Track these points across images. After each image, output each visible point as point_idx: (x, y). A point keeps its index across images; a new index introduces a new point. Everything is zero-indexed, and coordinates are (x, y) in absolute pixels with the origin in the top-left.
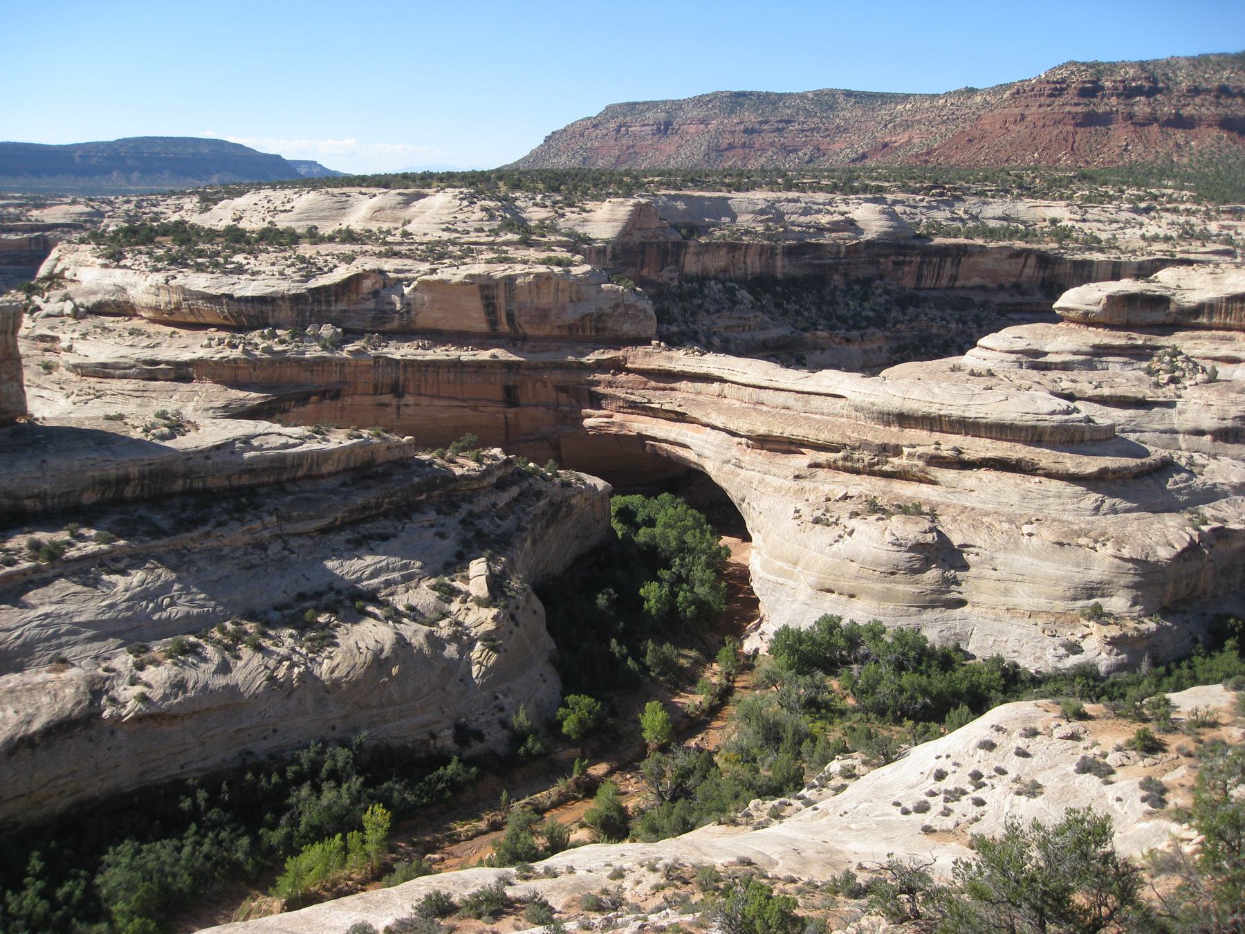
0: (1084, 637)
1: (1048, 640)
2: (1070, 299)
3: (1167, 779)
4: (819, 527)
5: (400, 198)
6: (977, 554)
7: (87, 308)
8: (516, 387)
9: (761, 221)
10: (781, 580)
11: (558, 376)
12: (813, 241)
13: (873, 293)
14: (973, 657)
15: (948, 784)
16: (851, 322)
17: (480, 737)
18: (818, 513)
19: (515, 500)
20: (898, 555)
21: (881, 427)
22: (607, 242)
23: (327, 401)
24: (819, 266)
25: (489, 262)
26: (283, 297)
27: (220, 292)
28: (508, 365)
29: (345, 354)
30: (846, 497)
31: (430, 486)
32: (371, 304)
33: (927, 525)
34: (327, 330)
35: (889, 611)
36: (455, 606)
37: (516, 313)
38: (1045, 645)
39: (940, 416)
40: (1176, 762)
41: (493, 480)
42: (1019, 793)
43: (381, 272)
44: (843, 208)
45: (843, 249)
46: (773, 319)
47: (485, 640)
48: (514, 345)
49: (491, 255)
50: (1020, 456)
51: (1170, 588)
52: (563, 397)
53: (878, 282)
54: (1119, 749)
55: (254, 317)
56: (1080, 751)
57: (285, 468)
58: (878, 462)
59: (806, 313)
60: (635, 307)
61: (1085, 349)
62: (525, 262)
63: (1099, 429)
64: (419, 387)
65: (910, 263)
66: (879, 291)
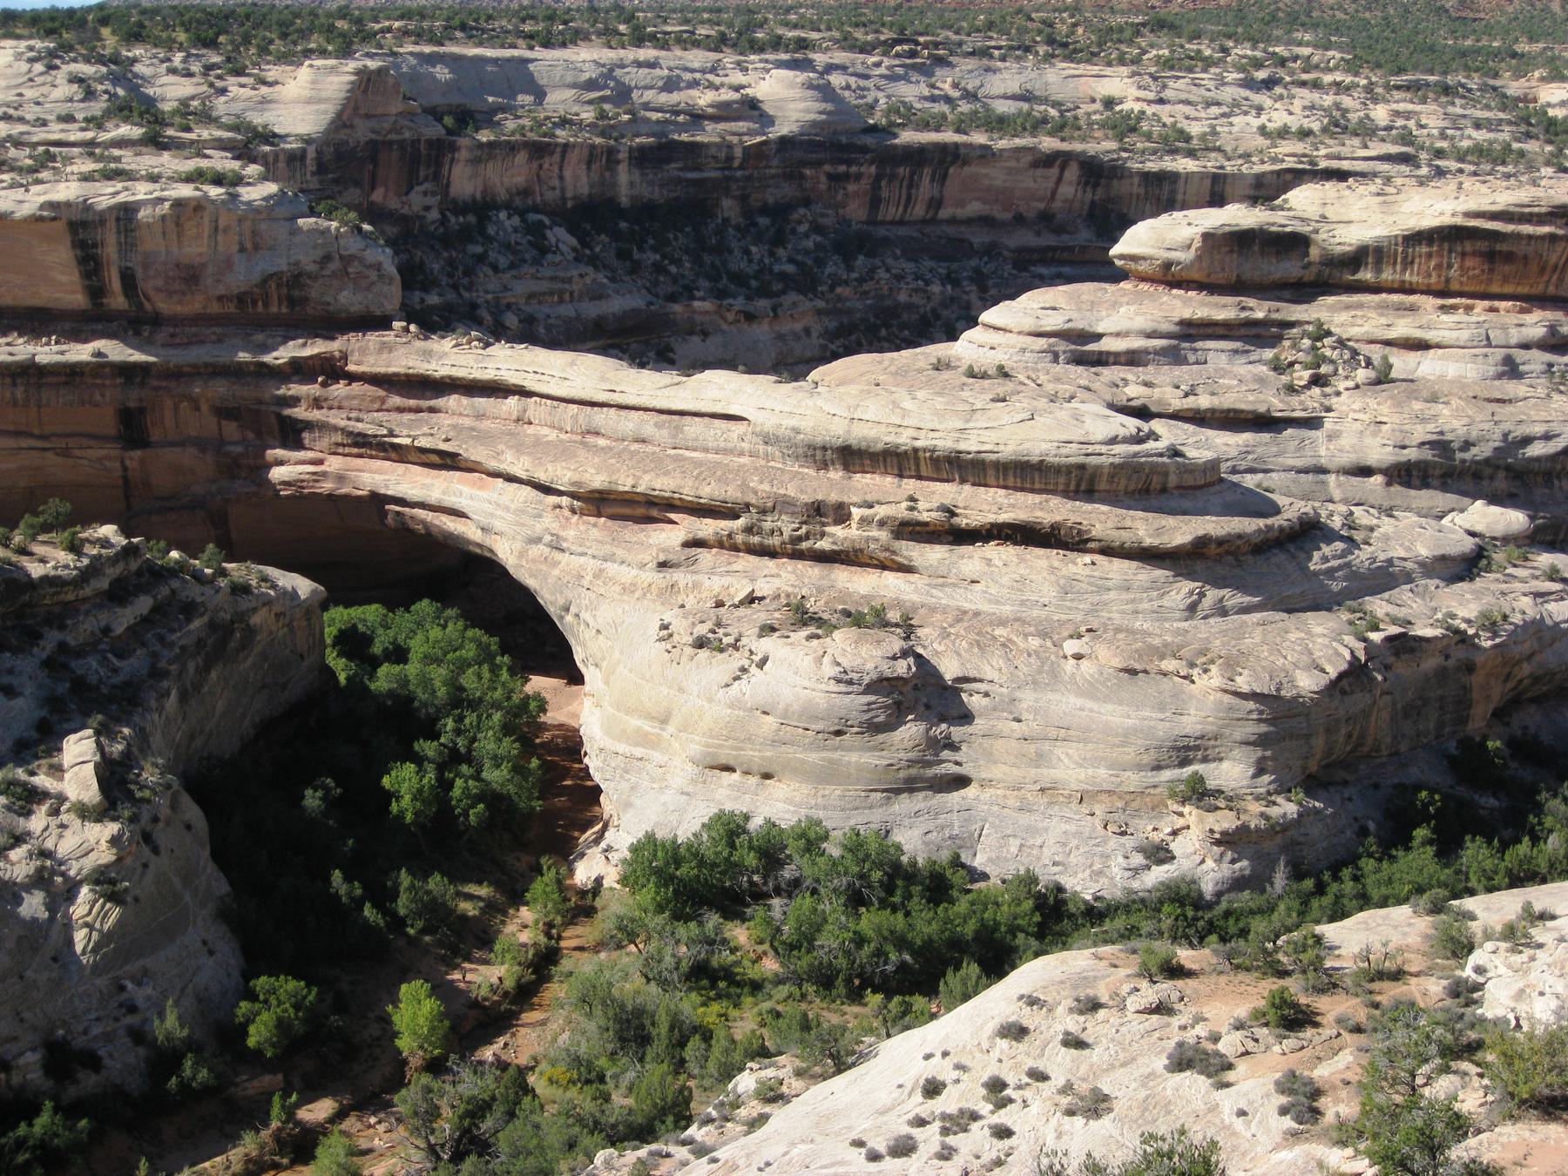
0: (1175, 833)
1: (1114, 842)
2: (1143, 239)
3: (1322, 1073)
4: (704, 654)
6: (987, 695)
9: (590, 102)
10: (639, 752)
12: (685, 137)
13: (793, 231)
15: (948, 1103)
16: (754, 283)
18: (702, 630)
19: (146, 621)
21: (812, 472)
22: (308, 140)
25: (86, 178)
28: (126, 371)
30: (751, 599)
36: (38, 821)
39: (916, 450)
40: (1336, 1043)
42: (1070, 1113)
44: (737, 78)
45: (738, 153)
47: (97, 882)
48: (137, 333)
49: (89, 166)
50: (1058, 518)
51: (1319, 742)
52: (231, 429)
53: (802, 211)
54: (1239, 1026)
56: (1174, 1031)
58: (808, 536)
59: (673, 269)
60: (361, 260)
61: (1166, 327)
62: (154, 178)
63: (1191, 469)
65: (858, 177)
66: (804, 228)
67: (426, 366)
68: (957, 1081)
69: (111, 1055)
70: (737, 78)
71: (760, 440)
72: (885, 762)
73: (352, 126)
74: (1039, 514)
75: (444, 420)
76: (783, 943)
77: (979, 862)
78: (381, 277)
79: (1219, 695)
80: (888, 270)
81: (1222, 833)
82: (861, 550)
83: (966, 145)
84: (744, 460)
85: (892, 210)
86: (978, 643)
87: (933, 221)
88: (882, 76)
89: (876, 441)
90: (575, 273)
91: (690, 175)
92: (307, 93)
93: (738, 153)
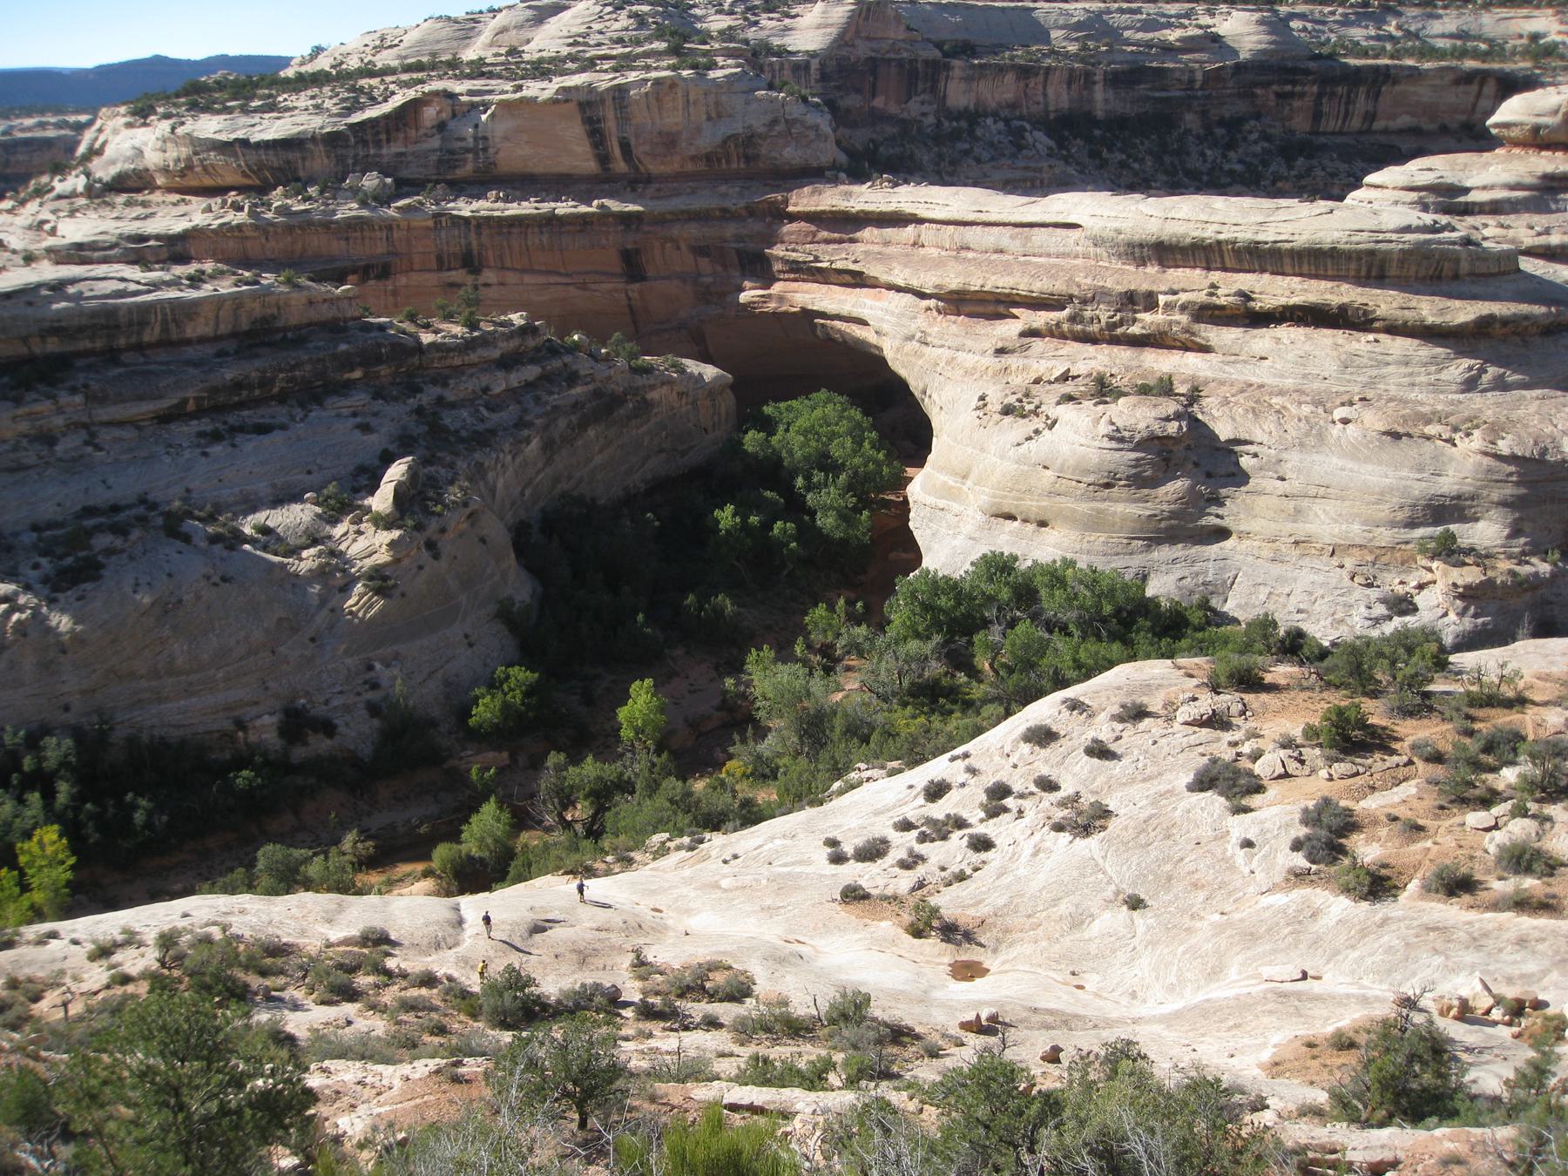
0: (1421, 587)
1: (1359, 592)
2: (1513, 110)
4: (1008, 419)
5: (529, 13)
6: (1255, 455)
7: (106, 184)
8: (637, 251)
9: (1076, 39)
10: (942, 503)
11: (693, 231)
12: (1154, 64)
13: (1245, 139)
14: (1236, 621)
16: (1205, 178)
17: (328, 728)
18: (1012, 399)
19: (529, 385)
20: (1118, 455)
21: (1132, 268)
22: (812, 55)
23: (372, 282)
24: (1161, 100)
26: (313, 139)
27: (233, 136)
28: (626, 219)
29: (391, 212)
30: (1065, 377)
31: (370, 359)
32: (435, 143)
33: (1171, 407)
34: (370, 181)
35: (1098, 546)
37: (633, 143)
38: (1351, 600)
39: (1219, 243)
40: (1401, 772)
41: (496, 354)
42: (1059, 828)
43: (450, 96)
44: (1205, 20)
45: (1199, 76)
46: (1081, 172)
47: (371, 578)
48: (634, 190)
50: (1345, 300)
52: (704, 262)
53: (1252, 123)
55: (280, 169)
57: (117, 327)
58: (1116, 321)
59: (1136, 166)
60: (802, 123)
61: (1528, 180)
63: (1486, 256)
64: (501, 257)
65: (1302, 95)
66: (1255, 136)
67: (846, 204)
68: (963, 785)
69: (347, 724)
70: (1205, 20)
71: (1090, 243)
72: (1148, 513)
73: (853, 46)
74: (1328, 296)
75: (859, 248)
76: (1005, 666)
77: (1230, 607)
78: (818, 136)
79: (1479, 457)
80: (1324, 169)
81: (1465, 587)
82: (1166, 333)
83: (1395, 66)
84: (1079, 261)
85: (1332, 123)
86: (1253, 409)
87: (1369, 131)
88: (1335, 22)
89: (1184, 236)
90: (1045, 165)
91: (1157, 94)
92: (819, 21)
93: (1199, 76)
